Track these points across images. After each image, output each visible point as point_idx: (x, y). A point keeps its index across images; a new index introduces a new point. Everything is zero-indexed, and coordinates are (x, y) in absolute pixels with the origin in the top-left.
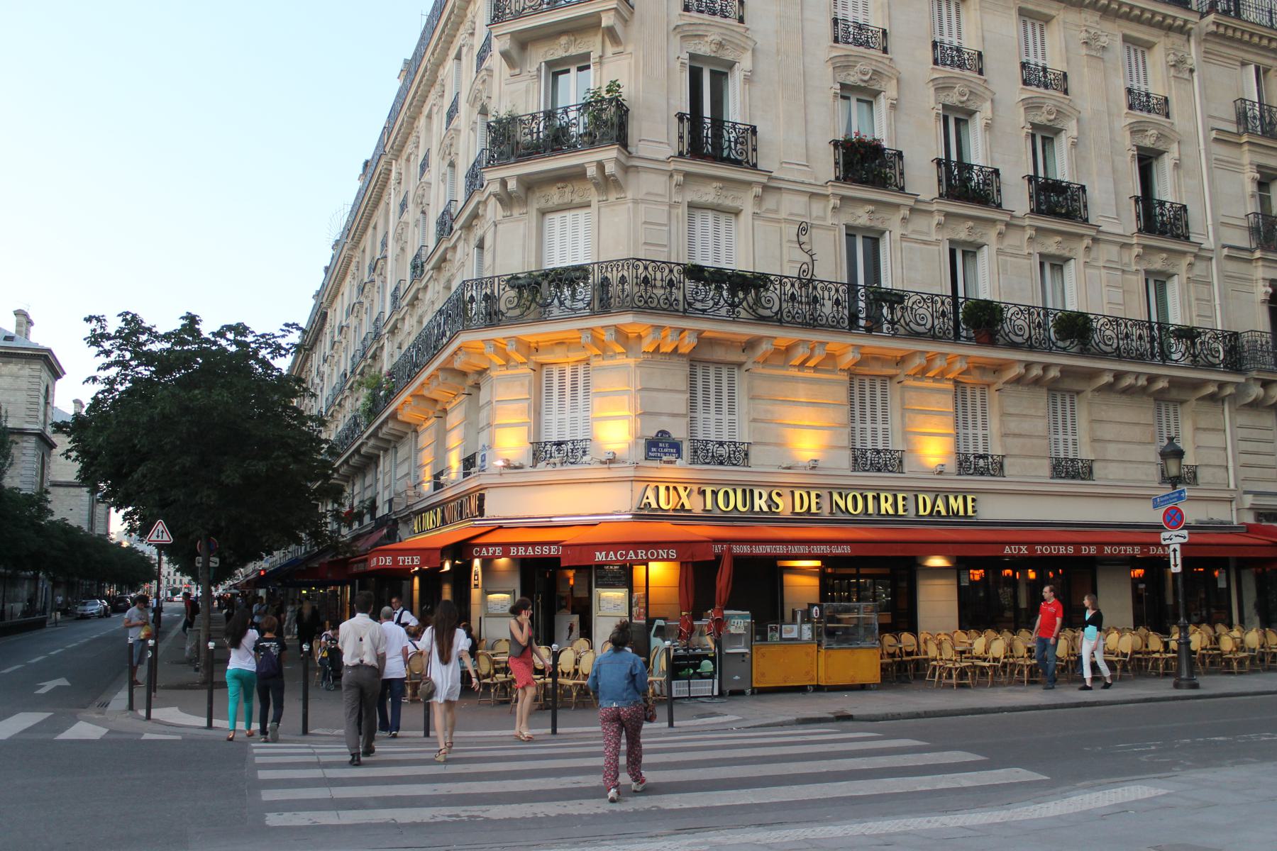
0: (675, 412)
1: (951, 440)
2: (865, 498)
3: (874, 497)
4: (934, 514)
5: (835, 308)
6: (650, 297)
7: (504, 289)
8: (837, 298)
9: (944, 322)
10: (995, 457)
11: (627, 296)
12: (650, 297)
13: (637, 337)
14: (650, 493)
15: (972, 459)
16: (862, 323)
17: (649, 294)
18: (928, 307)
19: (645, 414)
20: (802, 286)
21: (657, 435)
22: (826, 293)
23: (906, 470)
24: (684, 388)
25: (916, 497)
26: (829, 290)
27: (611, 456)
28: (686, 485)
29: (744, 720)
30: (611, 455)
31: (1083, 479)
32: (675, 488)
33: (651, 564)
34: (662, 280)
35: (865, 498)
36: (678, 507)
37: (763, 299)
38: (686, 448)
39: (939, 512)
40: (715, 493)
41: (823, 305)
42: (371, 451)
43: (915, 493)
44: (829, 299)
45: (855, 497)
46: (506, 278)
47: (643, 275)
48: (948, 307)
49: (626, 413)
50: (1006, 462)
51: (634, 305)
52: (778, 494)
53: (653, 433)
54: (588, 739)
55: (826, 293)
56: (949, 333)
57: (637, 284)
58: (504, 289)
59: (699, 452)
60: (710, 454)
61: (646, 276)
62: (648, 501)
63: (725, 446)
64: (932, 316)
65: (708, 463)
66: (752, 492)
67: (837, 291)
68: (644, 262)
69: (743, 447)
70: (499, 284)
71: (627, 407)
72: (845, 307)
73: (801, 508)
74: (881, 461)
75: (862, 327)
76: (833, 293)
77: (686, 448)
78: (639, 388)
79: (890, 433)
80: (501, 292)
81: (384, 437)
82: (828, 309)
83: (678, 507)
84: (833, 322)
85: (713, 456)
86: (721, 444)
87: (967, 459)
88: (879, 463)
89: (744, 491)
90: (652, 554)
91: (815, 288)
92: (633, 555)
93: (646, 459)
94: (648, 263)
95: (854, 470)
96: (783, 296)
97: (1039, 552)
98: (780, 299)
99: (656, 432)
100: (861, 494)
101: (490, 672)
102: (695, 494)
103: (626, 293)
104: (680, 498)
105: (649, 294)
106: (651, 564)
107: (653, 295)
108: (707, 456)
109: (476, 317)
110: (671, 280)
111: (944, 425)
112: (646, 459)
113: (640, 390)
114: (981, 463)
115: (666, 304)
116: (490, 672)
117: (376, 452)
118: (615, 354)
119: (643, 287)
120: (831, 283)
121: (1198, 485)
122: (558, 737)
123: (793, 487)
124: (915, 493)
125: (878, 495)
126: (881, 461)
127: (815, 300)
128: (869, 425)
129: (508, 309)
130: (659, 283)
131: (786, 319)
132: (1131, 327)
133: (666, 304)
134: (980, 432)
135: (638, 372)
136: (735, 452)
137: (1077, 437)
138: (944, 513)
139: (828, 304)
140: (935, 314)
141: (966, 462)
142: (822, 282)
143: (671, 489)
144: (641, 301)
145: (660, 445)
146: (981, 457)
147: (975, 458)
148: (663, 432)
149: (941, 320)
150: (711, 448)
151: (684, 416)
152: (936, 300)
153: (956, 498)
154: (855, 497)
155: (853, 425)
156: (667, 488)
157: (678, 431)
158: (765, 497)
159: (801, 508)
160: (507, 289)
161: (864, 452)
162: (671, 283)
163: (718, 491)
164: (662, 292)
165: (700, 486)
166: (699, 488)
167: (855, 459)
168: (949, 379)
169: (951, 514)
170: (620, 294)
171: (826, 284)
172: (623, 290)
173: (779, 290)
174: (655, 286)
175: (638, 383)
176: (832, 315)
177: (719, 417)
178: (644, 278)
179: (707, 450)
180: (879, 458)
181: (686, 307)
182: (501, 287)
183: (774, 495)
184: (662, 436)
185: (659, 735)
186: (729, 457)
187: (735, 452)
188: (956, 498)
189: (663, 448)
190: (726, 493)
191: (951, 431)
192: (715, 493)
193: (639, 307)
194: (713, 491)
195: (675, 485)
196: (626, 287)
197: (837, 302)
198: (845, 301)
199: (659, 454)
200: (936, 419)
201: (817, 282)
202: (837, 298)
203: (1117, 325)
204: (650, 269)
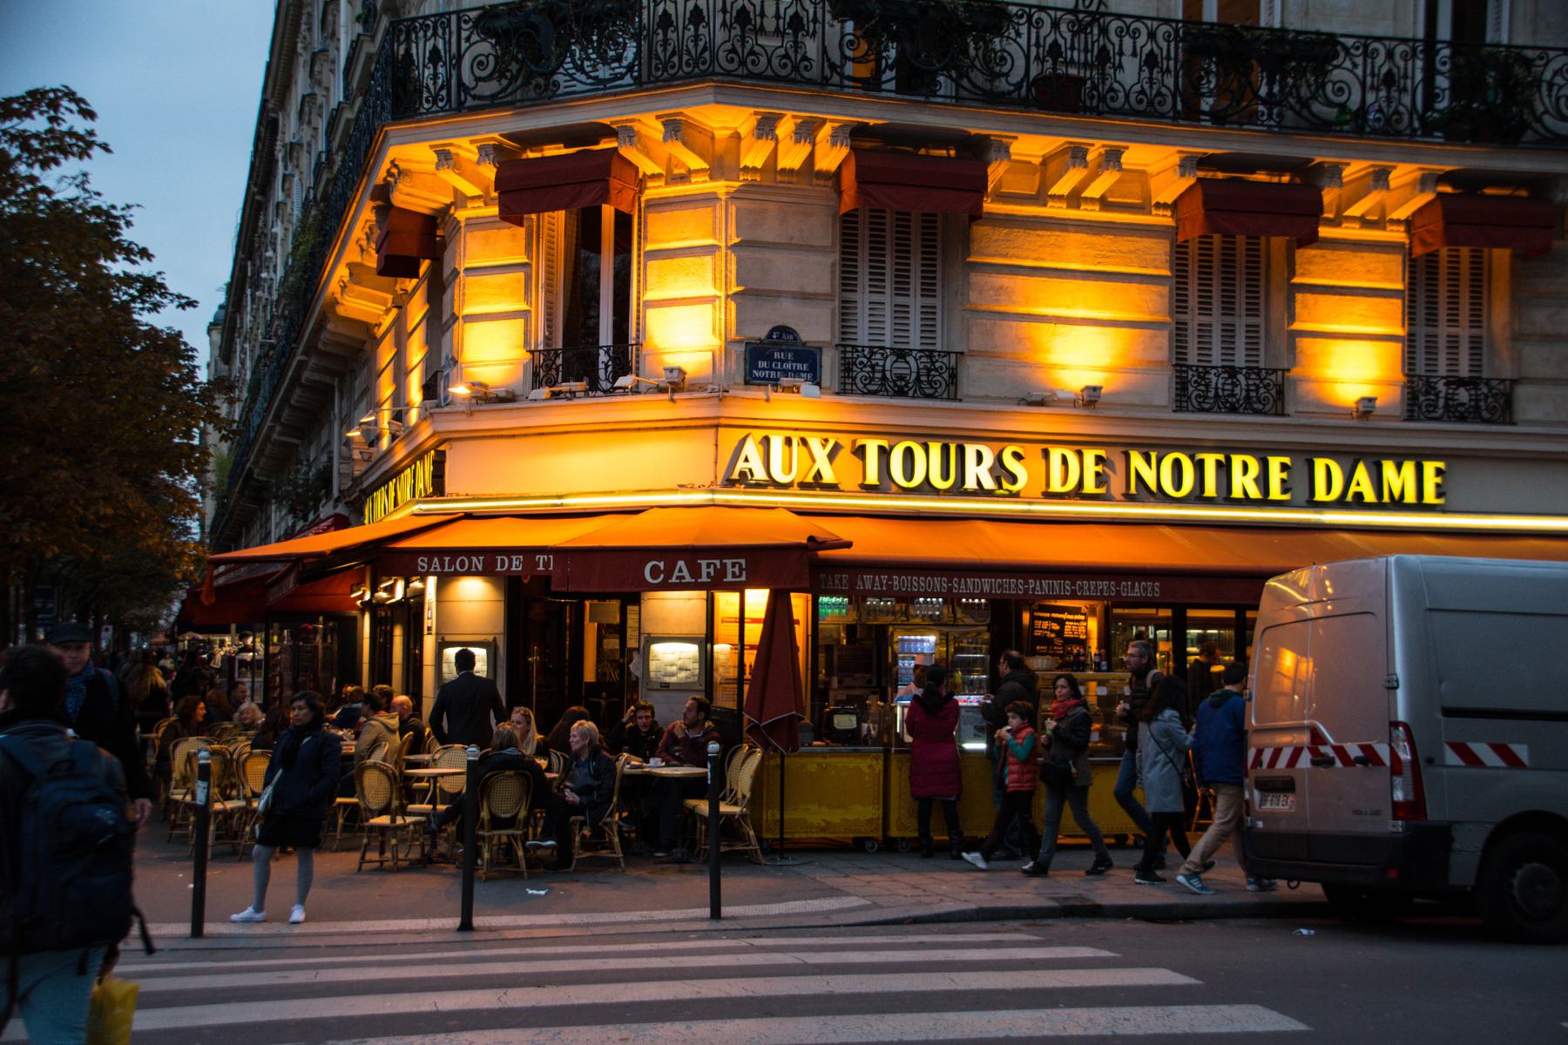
0: (810, 290)
1: (1395, 349)
2: (1199, 466)
3: (1218, 463)
4: (1349, 498)
5: (1146, 74)
6: (752, 52)
7: (468, 39)
8: (1055, 42)
9: (1151, 78)
10: (1494, 383)
11: (705, 49)
12: (752, 52)
13: (731, 136)
14: (752, 450)
15: (1441, 386)
16: (1207, 104)
17: (748, 46)
18: (1355, 65)
19: (748, 295)
20: (1079, 29)
21: (770, 336)
22: (1127, 42)
23: (1290, 409)
24: (827, 242)
25: (1046, 454)
26: (1135, 35)
27: (675, 377)
28: (825, 435)
29: (875, 906)
30: (675, 373)
31: (1257, 412)
32: (804, 442)
33: (748, 592)
34: (777, 16)
35: (1199, 466)
36: (810, 479)
37: (1329, 87)
38: (829, 363)
39: (1359, 496)
40: (884, 453)
41: (1121, 66)
42: (317, 377)
43: (1045, 446)
44: (1134, 54)
45: (1177, 464)
46: (473, 15)
47: (1050, 40)
48: (1164, 45)
49: (710, 291)
50: (1522, 392)
51: (718, 69)
52: (1018, 456)
53: (761, 332)
54: (533, 941)
55: (1127, 42)
56: (1399, 121)
57: (1037, 57)
58: (468, 39)
59: (1191, 389)
60: (878, 375)
61: (1152, 50)
62: (747, 465)
63: (909, 359)
64: (1363, 84)
65: (1208, 411)
66: (961, 452)
67: (1152, 35)
68: (1149, 23)
69: (1273, 377)
70: (459, 29)
71: (710, 276)
72: (1168, 71)
73: (1065, 481)
74: (1237, 390)
75: (1205, 113)
76: (1143, 39)
77: (829, 363)
78: (736, 240)
79: (1485, 346)
80: (464, 45)
81: (329, 349)
82: (1130, 74)
83: (810, 479)
84: (1140, 102)
85: (884, 378)
86: (901, 354)
87: (1430, 388)
88: (1233, 395)
89: (945, 450)
90: (462, 564)
91: (1104, 31)
92: (685, 573)
93: (747, 383)
94: (1059, 14)
95: (1180, 408)
96: (1034, 50)
97: (541, 568)
98: (1027, 57)
99: (768, 328)
100: (1192, 458)
101: (389, 803)
102: (845, 455)
103: (701, 44)
104: (814, 461)
105: (748, 46)
106: (748, 592)
107: (757, 49)
108: (872, 379)
109: (675, 59)
110: (1055, 43)
111: (1387, 319)
112: (747, 383)
113: (735, 245)
114: (1463, 395)
115: (732, 60)
116: (389, 803)
117: (327, 379)
118: (690, 172)
119: (737, 31)
120: (1138, 18)
121: (1513, 423)
122: (723, 925)
123: (1045, 443)
124: (1376, 459)
125: (1229, 460)
126: (1237, 390)
127: (1104, 55)
128: (1443, 330)
129: (478, 79)
130: (770, 24)
131: (724, 64)
132: (1405, 57)
133: (785, 66)
134: (1464, 332)
135: (733, 209)
136: (929, 370)
137: (1483, 332)
138: (1370, 497)
139: (1131, 66)
140: (1369, 80)
141: (1427, 393)
142: (1119, 17)
143: (795, 442)
144: (785, 66)
145: (777, 355)
146: (1461, 382)
147: (1447, 384)
148: (783, 330)
149: (1383, 93)
150: (1214, 379)
151: (827, 297)
152: (1376, 50)
153: (1399, 467)
154: (1177, 464)
155: (1182, 317)
156: (788, 442)
157: (815, 327)
158: (989, 459)
159: (1065, 481)
160: (475, 38)
161: (1203, 372)
162: (796, 23)
163: (892, 448)
164: (776, 42)
165: (854, 436)
166: (854, 442)
167: (1182, 386)
168: (1398, 222)
169: (1386, 499)
170: (691, 45)
171: (1129, 21)
172: (697, 37)
173: (1025, 36)
174: (761, 30)
175: (732, 230)
176: (1137, 88)
177: (901, 300)
178: (1051, 46)
179: (873, 367)
180: (1234, 385)
181: (827, 72)
182: (464, 34)
183: (1008, 460)
184: (779, 337)
185: (684, 935)
186: (918, 379)
187: (1258, 388)
188: (1399, 467)
189: (782, 362)
190: (909, 452)
191: (1399, 331)
192: (884, 453)
193: (728, 73)
194: (881, 448)
195: (803, 434)
196: (701, 30)
197: (1151, 61)
198: (1168, 58)
199: (773, 374)
200: (1363, 304)
201: (1109, 19)
202: (1055, 42)
203: (1365, 54)
204: (1063, 27)
